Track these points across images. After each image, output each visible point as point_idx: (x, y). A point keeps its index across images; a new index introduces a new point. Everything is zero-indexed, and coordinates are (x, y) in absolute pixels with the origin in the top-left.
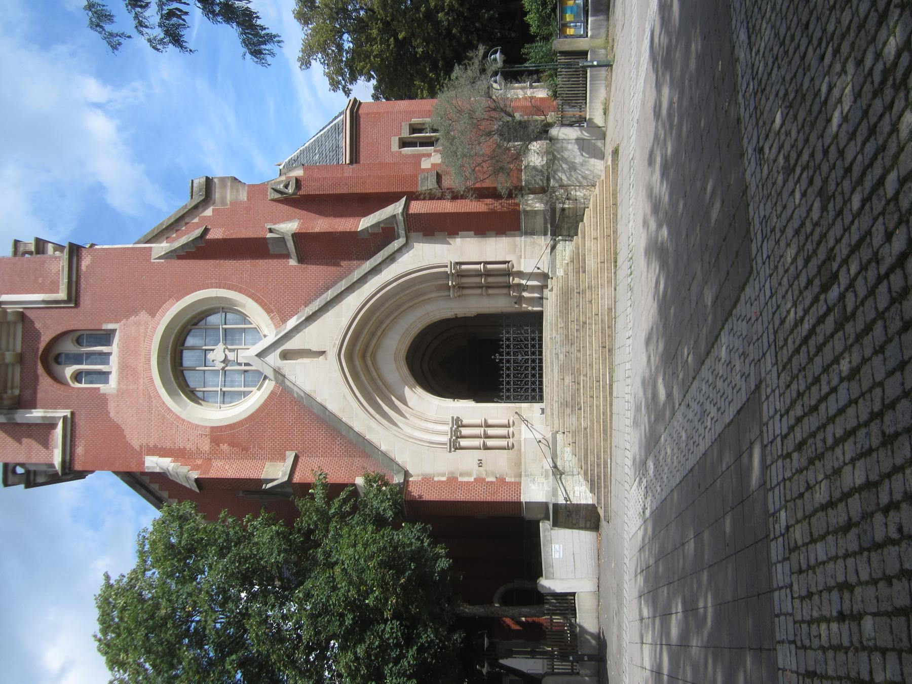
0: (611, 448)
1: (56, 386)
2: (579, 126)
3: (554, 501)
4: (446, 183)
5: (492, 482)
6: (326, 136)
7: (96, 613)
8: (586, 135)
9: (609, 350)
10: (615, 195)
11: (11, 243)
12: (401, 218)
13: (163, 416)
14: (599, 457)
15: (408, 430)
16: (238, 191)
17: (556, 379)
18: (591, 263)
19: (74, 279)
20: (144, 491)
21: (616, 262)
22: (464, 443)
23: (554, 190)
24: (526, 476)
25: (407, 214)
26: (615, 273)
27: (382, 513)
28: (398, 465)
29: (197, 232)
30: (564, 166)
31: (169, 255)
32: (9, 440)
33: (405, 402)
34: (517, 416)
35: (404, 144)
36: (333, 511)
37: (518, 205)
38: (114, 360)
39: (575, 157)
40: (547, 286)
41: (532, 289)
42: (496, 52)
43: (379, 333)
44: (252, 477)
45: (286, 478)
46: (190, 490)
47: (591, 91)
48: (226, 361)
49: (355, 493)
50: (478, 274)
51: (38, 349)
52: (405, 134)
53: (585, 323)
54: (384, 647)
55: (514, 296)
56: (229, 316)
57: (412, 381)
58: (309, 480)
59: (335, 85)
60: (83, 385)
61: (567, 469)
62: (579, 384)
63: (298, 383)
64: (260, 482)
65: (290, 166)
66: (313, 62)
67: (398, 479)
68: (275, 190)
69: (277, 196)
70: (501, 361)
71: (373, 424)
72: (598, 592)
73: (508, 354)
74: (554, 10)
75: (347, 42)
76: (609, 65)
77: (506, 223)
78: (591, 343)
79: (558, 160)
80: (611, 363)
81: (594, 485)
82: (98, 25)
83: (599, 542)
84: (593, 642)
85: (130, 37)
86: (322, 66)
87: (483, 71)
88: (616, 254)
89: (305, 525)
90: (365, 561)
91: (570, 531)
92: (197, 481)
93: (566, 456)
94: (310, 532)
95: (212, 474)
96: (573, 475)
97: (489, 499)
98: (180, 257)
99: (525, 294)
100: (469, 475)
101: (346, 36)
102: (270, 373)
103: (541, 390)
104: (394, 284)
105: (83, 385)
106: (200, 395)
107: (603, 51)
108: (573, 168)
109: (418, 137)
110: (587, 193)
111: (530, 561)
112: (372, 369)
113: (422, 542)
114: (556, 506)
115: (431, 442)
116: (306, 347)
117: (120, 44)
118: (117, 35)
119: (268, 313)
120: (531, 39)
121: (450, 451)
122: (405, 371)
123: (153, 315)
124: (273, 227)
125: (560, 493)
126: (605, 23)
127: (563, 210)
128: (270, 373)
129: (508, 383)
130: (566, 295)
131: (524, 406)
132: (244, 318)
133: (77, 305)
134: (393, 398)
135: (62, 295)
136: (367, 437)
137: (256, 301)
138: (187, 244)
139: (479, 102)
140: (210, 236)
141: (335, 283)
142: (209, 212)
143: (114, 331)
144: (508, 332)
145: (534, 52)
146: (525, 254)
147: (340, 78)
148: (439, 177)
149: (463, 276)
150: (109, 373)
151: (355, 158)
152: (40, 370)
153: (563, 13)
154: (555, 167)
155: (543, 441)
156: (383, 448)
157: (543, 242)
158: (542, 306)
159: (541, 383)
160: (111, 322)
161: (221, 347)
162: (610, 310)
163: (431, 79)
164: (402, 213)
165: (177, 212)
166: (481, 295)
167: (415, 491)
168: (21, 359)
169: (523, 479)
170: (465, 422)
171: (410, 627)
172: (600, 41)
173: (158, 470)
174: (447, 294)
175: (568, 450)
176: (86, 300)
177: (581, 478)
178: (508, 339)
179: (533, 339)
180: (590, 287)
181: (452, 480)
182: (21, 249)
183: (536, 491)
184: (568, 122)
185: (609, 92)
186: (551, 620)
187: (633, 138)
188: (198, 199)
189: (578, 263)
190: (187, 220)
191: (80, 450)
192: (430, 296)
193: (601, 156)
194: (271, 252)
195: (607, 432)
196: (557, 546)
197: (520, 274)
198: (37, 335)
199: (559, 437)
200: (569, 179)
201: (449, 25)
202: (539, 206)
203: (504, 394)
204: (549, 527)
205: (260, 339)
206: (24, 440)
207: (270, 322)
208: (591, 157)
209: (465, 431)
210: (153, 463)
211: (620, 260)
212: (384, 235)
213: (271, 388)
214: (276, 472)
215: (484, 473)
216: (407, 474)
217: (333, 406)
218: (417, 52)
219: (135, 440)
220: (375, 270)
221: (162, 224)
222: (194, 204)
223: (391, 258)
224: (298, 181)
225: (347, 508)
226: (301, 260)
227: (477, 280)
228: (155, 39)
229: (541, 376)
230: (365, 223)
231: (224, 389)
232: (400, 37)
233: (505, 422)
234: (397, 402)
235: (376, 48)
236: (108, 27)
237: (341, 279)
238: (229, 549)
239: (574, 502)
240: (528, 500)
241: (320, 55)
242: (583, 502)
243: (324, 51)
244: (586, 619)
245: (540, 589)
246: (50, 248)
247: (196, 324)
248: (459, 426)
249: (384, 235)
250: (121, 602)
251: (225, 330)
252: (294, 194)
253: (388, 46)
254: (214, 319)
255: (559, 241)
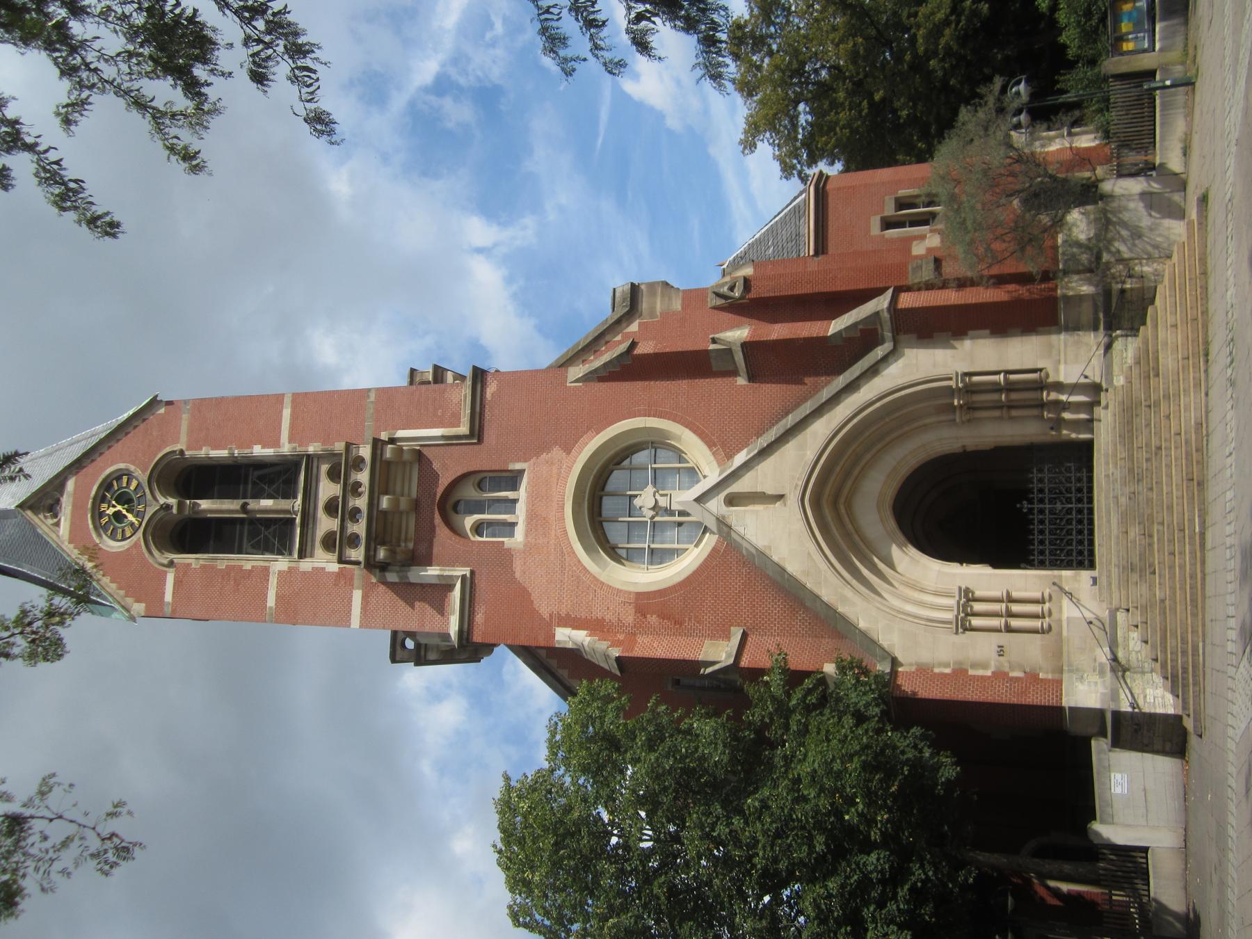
0: (1204, 625)
1: (454, 538)
2: (1146, 175)
3: (1113, 707)
4: (949, 270)
5: (1017, 679)
6: (784, 221)
7: (495, 819)
8: (1156, 186)
9: (1198, 483)
10: (1203, 260)
11: (408, 371)
12: (886, 315)
13: (578, 577)
14: (1184, 641)
15: (896, 603)
16: (670, 299)
17: (1115, 532)
18: (1168, 361)
19: (478, 409)
20: (549, 678)
21: (1207, 355)
22: (976, 622)
23: (1108, 266)
24: (1070, 671)
25: (896, 310)
26: (1206, 371)
27: (862, 709)
28: (883, 649)
29: (623, 347)
30: (1124, 233)
31: (586, 378)
32: (401, 603)
33: (892, 566)
34: (1056, 588)
35: (888, 224)
36: (794, 702)
37: (1055, 289)
38: (521, 508)
39: (1140, 220)
40: (1099, 403)
41: (1078, 407)
42: (1018, 83)
43: (856, 472)
44: (687, 657)
45: (731, 661)
46: (610, 672)
47: (1162, 124)
48: (656, 507)
49: (823, 681)
50: (996, 388)
51: (435, 494)
52: (890, 210)
53: (1160, 448)
54: (865, 883)
55: (1049, 419)
56: (661, 453)
57: (902, 538)
58: (761, 665)
59: (787, 170)
60: (484, 539)
61: (1134, 663)
62: (1151, 536)
63: (748, 536)
64: (695, 665)
65: (737, 264)
66: (759, 144)
67: (884, 667)
68: (718, 295)
69: (720, 302)
70: (1031, 511)
71: (848, 593)
72: (1186, 849)
73: (1041, 501)
74: (1103, 20)
75: (804, 116)
76: (1189, 83)
77: (1034, 313)
78: (1170, 476)
79: (1114, 224)
80: (1203, 502)
81: (1176, 683)
82: (552, 51)
83: (1187, 774)
84: (1178, 925)
85: (585, 60)
86: (770, 148)
87: (1001, 110)
88: (1207, 343)
89: (757, 718)
90: (842, 763)
91: (1139, 754)
92: (618, 659)
93: (1132, 644)
94: (766, 726)
95: (638, 652)
96: (1143, 673)
97: (1015, 700)
98: (602, 379)
99: (1067, 415)
100: (985, 666)
101: (801, 107)
102: (712, 524)
103: (1092, 553)
104: (878, 405)
105: (484, 539)
106: (623, 553)
107: (1179, 68)
108: (1137, 234)
109: (909, 214)
110: (1160, 267)
111: (1079, 797)
112: (846, 519)
113: (921, 751)
114: (1117, 715)
115: (929, 618)
116: (759, 490)
117: (574, 70)
118: (572, 59)
119: (710, 447)
120: (1071, 65)
121: (957, 633)
122: (892, 524)
123: (568, 450)
124: (716, 336)
125: (1122, 696)
126: (1183, 28)
127: (1123, 291)
128: (712, 524)
129: (1042, 542)
130: (1129, 411)
131: (1066, 573)
132: (680, 455)
133: (480, 441)
134: (876, 560)
135: (464, 429)
136: (840, 610)
137: (695, 432)
138: (610, 362)
139: (997, 158)
140: (639, 351)
141: (797, 405)
142: (634, 327)
143: (521, 472)
144: (1041, 471)
145: (1073, 85)
146: (1068, 358)
147: (795, 161)
148: (938, 262)
149: (973, 392)
150: (513, 525)
151: (821, 247)
152: (438, 519)
153: (1117, 21)
154: (1109, 235)
155: (1095, 622)
156: (862, 625)
157: (1092, 340)
158: (1092, 431)
159: (1091, 543)
160: (519, 461)
161: (650, 489)
162: (1199, 425)
163: (921, 150)
164: (889, 309)
165: (596, 329)
166: (1001, 418)
167: (907, 686)
168: (416, 505)
169: (1065, 676)
170: (978, 594)
171: (903, 857)
172: (1175, 55)
173: (570, 645)
174: (951, 417)
175: (1135, 635)
176: (490, 434)
177: (1158, 679)
178: (1041, 491)
179: (1079, 480)
180: (1167, 397)
181: (960, 673)
182: (417, 379)
183: (1085, 692)
184: (1125, 172)
185: (1190, 125)
186: (1111, 895)
187: (1231, 169)
188: (621, 311)
189: (1148, 365)
190: (608, 338)
191: (479, 618)
192: (927, 421)
193: (1180, 214)
194: (714, 369)
195: (1197, 601)
196: (1118, 776)
197: (1059, 387)
198: (436, 477)
199: (1121, 616)
200: (1131, 250)
201: (945, 75)
202: (1086, 289)
203: (1036, 557)
204: (1105, 747)
205: (698, 481)
206: (417, 604)
207: (712, 458)
208: (1163, 217)
209: (978, 607)
210: (566, 636)
211: (1214, 350)
212: (863, 340)
213: (713, 544)
214: (719, 653)
215: (1006, 665)
216: (895, 662)
217: (793, 568)
218: (899, 117)
219: (544, 608)
220: (852, 387)
221: (578, 344)
222: (616, 317)
223: (874, 371)
224: (746, 281)
225: (812, 699)
226: (752, 378)
227: (995, 396)
228: (611, 61)
229: (1091, 532)
230: (836, 326)
231: (653, 546)
232: (877, 97)
233: (1037, 595)
234: (881, 565)
235: (843, 116)
236: (562, 53)
237: (804, 399)
238: (663, 740)
239: (1146, 710)
240: (1073, 705)
241: (768, 135)
242: (1160, 710)
243: (773, 129)
244: (1166, 889)
245: (1092, 837)
246: (449, 377)
247: (619, 463)
248: (969, 600)
249: (863, 340)
250: (524, 805)
251: (655, 470)
252: (742, 297)
253: (860, 112)
254: (641, 458)
255: (1117, 337)
